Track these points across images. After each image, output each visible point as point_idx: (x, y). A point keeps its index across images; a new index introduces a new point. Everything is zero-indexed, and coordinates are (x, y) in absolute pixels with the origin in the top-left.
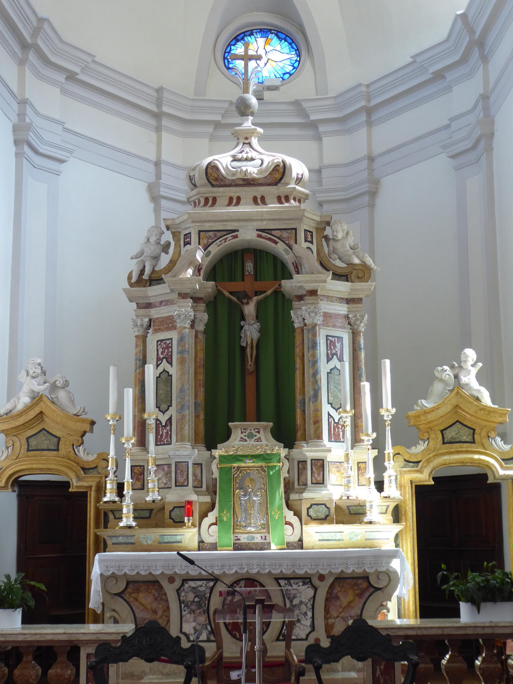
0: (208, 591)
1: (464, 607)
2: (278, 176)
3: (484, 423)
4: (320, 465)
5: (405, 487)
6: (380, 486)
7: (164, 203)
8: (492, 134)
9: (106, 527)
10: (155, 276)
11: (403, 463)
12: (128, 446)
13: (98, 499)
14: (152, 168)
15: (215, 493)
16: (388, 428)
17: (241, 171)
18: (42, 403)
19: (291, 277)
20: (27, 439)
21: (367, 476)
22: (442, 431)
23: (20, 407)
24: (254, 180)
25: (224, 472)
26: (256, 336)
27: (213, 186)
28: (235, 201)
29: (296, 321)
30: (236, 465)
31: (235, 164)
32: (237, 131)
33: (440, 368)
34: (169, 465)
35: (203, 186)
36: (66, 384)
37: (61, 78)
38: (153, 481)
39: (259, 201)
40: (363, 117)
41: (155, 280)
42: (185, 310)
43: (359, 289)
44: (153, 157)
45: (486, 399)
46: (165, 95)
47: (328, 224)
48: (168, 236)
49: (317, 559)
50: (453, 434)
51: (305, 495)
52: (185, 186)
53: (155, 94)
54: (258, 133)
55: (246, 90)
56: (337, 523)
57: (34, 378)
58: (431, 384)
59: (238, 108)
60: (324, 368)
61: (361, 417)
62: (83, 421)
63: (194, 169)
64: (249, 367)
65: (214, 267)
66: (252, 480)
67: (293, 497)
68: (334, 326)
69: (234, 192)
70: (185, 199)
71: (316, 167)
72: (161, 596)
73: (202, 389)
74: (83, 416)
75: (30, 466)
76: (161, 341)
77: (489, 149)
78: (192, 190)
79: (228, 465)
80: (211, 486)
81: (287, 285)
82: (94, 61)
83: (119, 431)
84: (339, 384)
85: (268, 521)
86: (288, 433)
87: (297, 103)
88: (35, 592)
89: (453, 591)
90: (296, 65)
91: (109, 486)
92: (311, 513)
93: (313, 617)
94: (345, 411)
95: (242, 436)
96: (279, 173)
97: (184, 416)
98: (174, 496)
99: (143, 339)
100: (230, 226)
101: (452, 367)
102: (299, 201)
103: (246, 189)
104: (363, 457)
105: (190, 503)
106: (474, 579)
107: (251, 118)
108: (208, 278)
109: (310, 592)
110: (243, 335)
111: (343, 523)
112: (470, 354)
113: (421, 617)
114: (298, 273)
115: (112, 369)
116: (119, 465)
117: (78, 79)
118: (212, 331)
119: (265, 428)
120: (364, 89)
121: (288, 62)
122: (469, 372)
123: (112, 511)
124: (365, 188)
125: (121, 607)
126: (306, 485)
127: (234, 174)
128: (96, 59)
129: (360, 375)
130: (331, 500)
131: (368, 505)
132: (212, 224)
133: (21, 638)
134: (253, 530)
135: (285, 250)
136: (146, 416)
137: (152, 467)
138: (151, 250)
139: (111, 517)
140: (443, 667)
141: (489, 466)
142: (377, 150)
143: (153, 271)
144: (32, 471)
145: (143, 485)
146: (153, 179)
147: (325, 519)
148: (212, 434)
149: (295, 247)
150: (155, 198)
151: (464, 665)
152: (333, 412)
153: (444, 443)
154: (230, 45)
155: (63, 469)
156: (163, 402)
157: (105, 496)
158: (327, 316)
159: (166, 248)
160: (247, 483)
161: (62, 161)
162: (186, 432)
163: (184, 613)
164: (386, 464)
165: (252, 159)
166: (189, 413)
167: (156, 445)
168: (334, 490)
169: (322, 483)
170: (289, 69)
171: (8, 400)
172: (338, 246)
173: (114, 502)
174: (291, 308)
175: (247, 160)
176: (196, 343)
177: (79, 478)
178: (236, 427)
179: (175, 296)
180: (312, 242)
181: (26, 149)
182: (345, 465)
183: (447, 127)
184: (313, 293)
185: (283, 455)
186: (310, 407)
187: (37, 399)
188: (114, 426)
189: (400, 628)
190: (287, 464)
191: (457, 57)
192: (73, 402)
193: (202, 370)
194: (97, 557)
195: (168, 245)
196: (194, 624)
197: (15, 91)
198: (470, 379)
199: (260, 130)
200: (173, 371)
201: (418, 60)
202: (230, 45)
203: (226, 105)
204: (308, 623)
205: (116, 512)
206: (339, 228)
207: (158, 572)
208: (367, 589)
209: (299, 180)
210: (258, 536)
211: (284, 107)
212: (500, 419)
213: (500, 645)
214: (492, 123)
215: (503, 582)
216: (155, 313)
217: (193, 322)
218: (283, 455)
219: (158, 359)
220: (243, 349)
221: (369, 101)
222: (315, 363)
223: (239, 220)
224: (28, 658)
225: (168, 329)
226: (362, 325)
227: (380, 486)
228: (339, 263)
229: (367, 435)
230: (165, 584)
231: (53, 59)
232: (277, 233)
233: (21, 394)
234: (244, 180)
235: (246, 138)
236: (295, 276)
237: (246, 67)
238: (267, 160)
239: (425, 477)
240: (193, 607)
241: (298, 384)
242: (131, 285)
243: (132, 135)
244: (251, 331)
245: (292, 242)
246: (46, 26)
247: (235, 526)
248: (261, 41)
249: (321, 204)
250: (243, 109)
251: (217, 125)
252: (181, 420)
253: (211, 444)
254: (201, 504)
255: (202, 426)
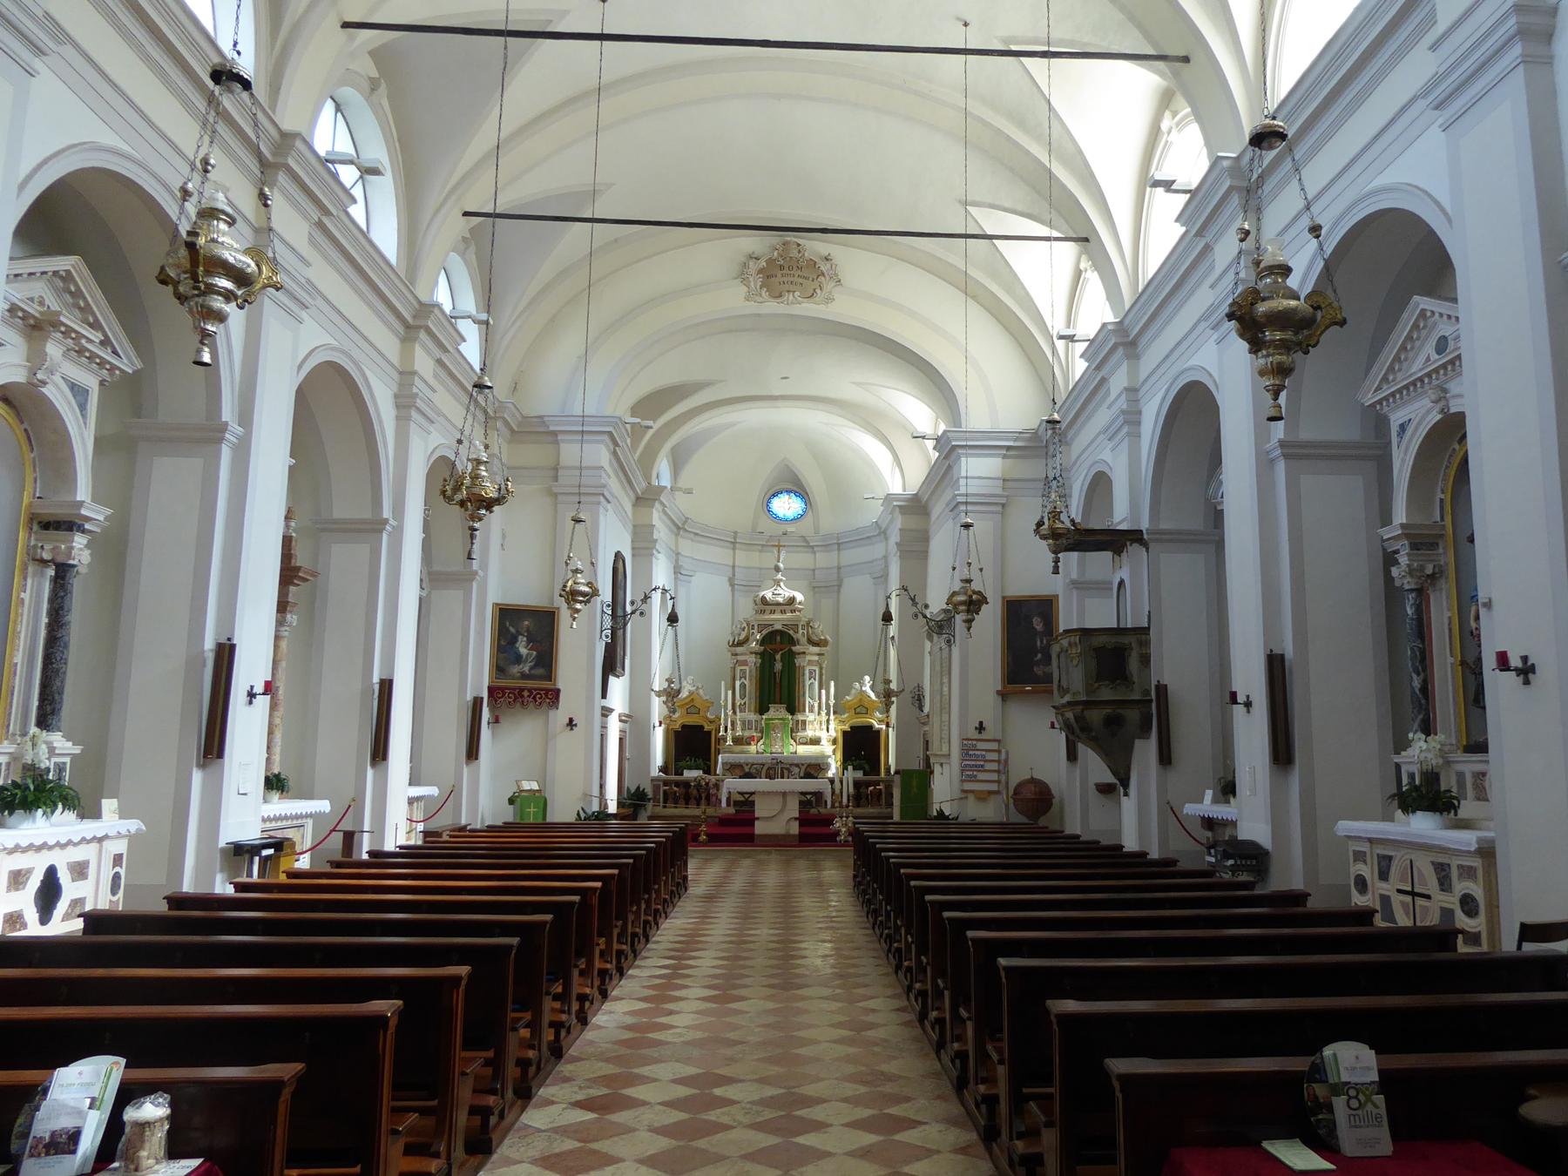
4: (804, 722)
41: (740, 644)
42: (752, 659)
49: (801, 757)
60: (808, 683)
86: (792, 710)
96: (792, 600)
98: (747, 734)
112: (867, 678)
148: (762, 709)
156: (743, 696)
168: (810, 733)
187: (691, 693)
198: (867, 688)
239: (847, 728)
243: (721, 555)
244: (778, 666)
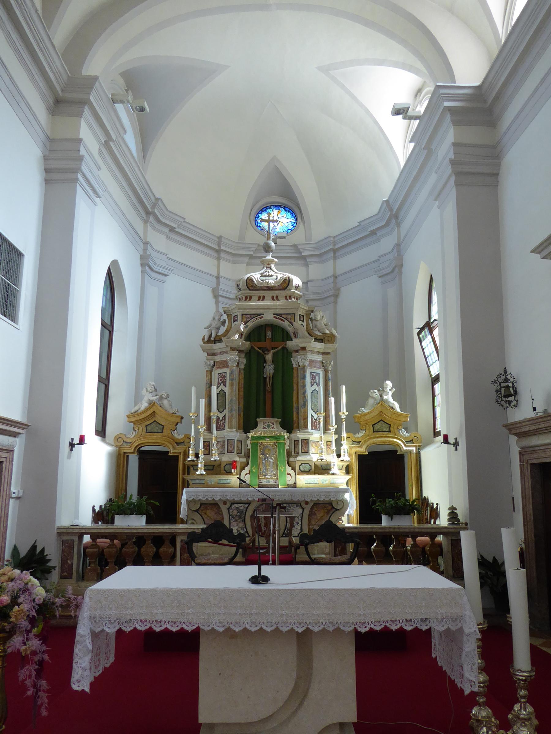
0: (245, 509)
1: (384, 518)
2: (285, 285)
3: (396, 421)
5: (352, 455)
6: (339, 456)
7: (220, 299)
8: (402, 265)
9: (188, 474)
10: (217, 338)
11: (351, 442)
12: (202, 430)
13: (185, 459)
14: (214, 280)
15: (249, 457)
16: (344, 423)
17: (266, 282)
18: (154, 407)
19: (292, 340)
20: (146, 426)
21: (332, 449)
22: (373, 425)
23: (143, 408)
24: (272, 287)
25: (254, 445)
26: (272, 371)
27: (250, 290)
28: (262, 298)
29: (294, 364)
30: (260, 441)
31: (262, 278)
32: (263, 261)
33: (372, 391)
34: (224, 442)
35: (244, 290)
36: (168, 397)
37: (167, 230)
38: (215, 450)
39: (275, 298)
40: (331, 254)
41: (218, 340)
42: (233, 357)
43: (329, 347)
44: (216, 275)
45: (398, 409)
46: (223, 240)
47: (312, 311)
48: (225, 317)
50: (379, 427)
51: (298, 458)
52: (235, 290)
53: (217, 240)
54: (276, 262)
55: (269, 239)
56: (315, 474)
57: (150, 392)
58: (367, 400)
59: (264, 248)
60: (309, 389)
61: (329, 417)
62: (177, 417)
63: (240, 281)
64: (268, 389)
65: (250, 334)
66: (269, 450)
67: (291, 459)
68: (315, 367)
69: (261, 293)
70: (235, 297)
71: (305, 281)
72: (219, 511)
73: (242, 400)
74: (177, 414)
75: (147, 441)
76: (221, 373)
77: (400, 273)
78: (238, 292)
79: (257, 441)
80: (246, 453)
81: (289, 344)
82: (184, 221)
83: (197, 422)
84: (317, 399)
85: (277, 472)
86: (289, 425)
87: (295, 246)
88: (154, 507)
89: (378, 509)
90: (295, 225)
91: (191, 452)
92: (301, 468)
93: (302, 525)
94: (320, 413)
95: (264, 426)
96: (286, 284)
97: (232, 415)
98: (226, 458)
99: (211, 372)
100: (259, 312)
101: (379, 391)
102: (297, 299)
103: (268, 292)
104: (329, 439)
105: (235, 462)
106: (389, 502)
107: (271, 253)
108: (247, 339)
109: (300, 511)
110: (265, 371)
111: (318, 474)
112: (389, 383)
113: (360, 523)
114: (296, 337)
115: (193, 388)
116: (197, 440)
117: (175, 230)
118: (248, 367)
119: (276, 422)
120: (332, 239)
121: (290, 223)
122: (388, 394)
123: (192, 466)
124: (332, 292)
125: (197, 517)
126: (298, 453)
127: (261, 284)
128: (186, 220)
129: (329, 394)
130: (312, 461)
131: (332, 464)
132: (249, 310)
133: (145, 531)
134: (269, 477)
135: (289, 325)
136: (212, 414)
137: (215, 443)
138: (214, 324)
139: (192, 469)
140: (372, 551)
141: (398, 445)
142: (339, 272)
143: (217, 336)
144: (148, 444)
145: (209, 452)
146: (215, 286)
147: (308, 472)
148: (248, 425)
149: (294, 323)
150: (216, 296)
151: (384, 549)
152: (314, 414)
153: (374, 432)
154: (258, 213)
155: (166, 443)
156: (221, 407)
157: (188, 457)
158: (311, 361)
159: (223, 323)
160: (266, 451)
161: (166, 275)
162: (233, 423)
163: (231, 521)
164: (342, 442)
165: (272, 276)
166: (235, 413)
167: (217, 430)
168: (314, 457)
169: (307, 452)
170: (291, 227)
171: (135, 406)
172: (318, 323)
173: (194, 461)
174: (291, 357)
175: (269, 276)
176: (239, 375)
177: (174, 448)
178: (261, 421)
179: (228, 349)
180: (303, 321)
181: (147, 268)
182: (320, 443)
183: (377, 260)
184: (304, 349)
185: (286, 437)
186: (301, 411)
187: (152, 404)
188: (194, 419)
189: (349, 528)
190: (288, 442)
191: (383, 223)
192: (171, 406)
193: (242, 390)
194: (185, 490)
195: (225, 321)
196: (237, 527)
197: (142, 237)
198: (389, 397)
199: (276, 260)
200: (227, 390)
201: (362, 224)
202: (258, 213)
203: (256, 246)
204: (299, 527)
205: (195, 466)
206: (318, 314)
207: (218, 499)
208: (331, 509)
209: (297, 287)
210: (272, 480)
211: (288, 248)
212: (404, 419)
213: (403, 542)
214: (402, 259)
215: (405, 505)
216: (218, 358)
217: (238, 363)
218: (286, 437)
219: (218, 383)
220: (265, 379)
221: (335, 245)
222: (304, 386)
223: (264, 309)
224: (149, 542)
225: (224, 367)
226: (330, 366)
227: (339, 456)
228: (317, 333)
229: (332, 426)
230: (221, 505)
231: (163, 220)
232: (285, 316)
233: (143, 401)
234: (267, 287)
235: (268, 265)
236: (294, 339)
237: (269, 225)
238: (280, 276)
239: (363, 450)
240: (237, 518)
241: (295, 398)
242: (204, 343)
243: (205, 262)
244: (269, 369)
245: (293, 321)
246: (160, 203)
247: (260, 475)
248: (276, 212)
249: (307, 301)
250: (267, 249)
251: (251, 257)
252: (230, 417)
253: (246, 430)
254: (241, 463)
255: (242, 421)
